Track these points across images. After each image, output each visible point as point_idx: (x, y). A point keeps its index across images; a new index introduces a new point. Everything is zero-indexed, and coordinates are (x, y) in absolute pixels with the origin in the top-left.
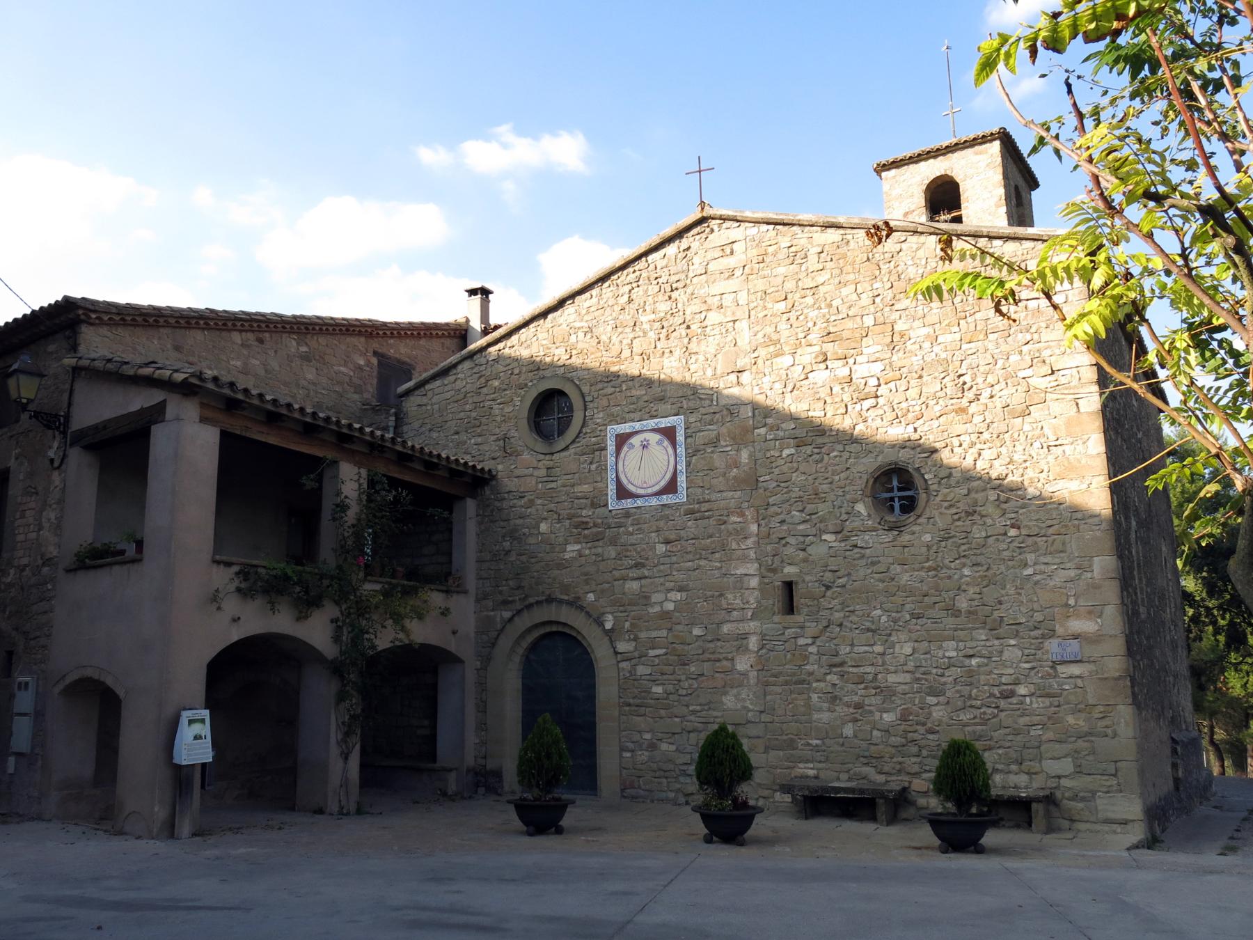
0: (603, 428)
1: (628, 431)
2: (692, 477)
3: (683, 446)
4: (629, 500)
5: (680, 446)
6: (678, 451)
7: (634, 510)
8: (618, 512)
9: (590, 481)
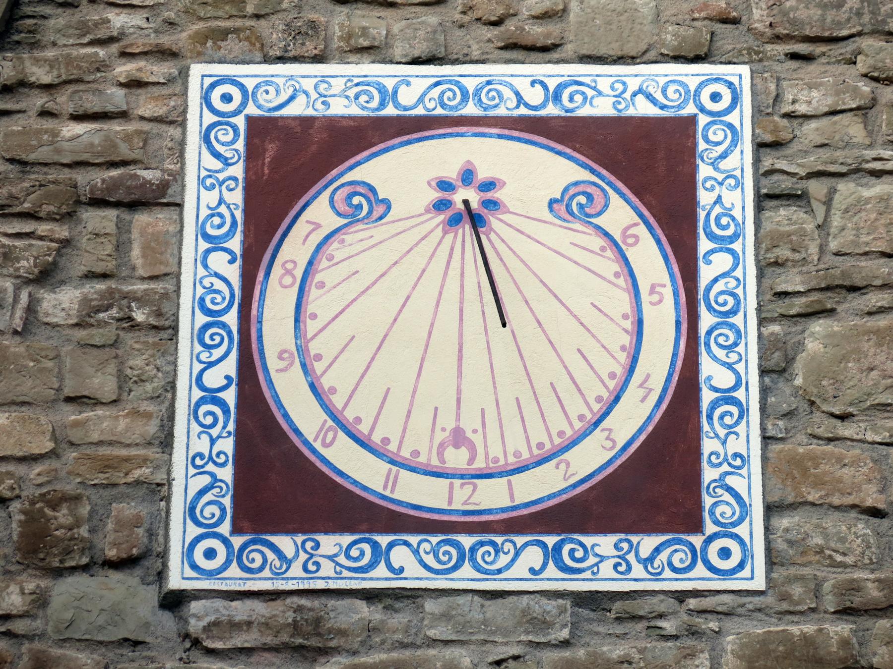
0: (157, 71)
1: (339, 108)
2: (800, 445)
3: (747, 246)
4: (330, 543)
5: (724, 244)
6: (706, 274)
7: (364, 610)
8: (240, 610)
9: (27, 387)
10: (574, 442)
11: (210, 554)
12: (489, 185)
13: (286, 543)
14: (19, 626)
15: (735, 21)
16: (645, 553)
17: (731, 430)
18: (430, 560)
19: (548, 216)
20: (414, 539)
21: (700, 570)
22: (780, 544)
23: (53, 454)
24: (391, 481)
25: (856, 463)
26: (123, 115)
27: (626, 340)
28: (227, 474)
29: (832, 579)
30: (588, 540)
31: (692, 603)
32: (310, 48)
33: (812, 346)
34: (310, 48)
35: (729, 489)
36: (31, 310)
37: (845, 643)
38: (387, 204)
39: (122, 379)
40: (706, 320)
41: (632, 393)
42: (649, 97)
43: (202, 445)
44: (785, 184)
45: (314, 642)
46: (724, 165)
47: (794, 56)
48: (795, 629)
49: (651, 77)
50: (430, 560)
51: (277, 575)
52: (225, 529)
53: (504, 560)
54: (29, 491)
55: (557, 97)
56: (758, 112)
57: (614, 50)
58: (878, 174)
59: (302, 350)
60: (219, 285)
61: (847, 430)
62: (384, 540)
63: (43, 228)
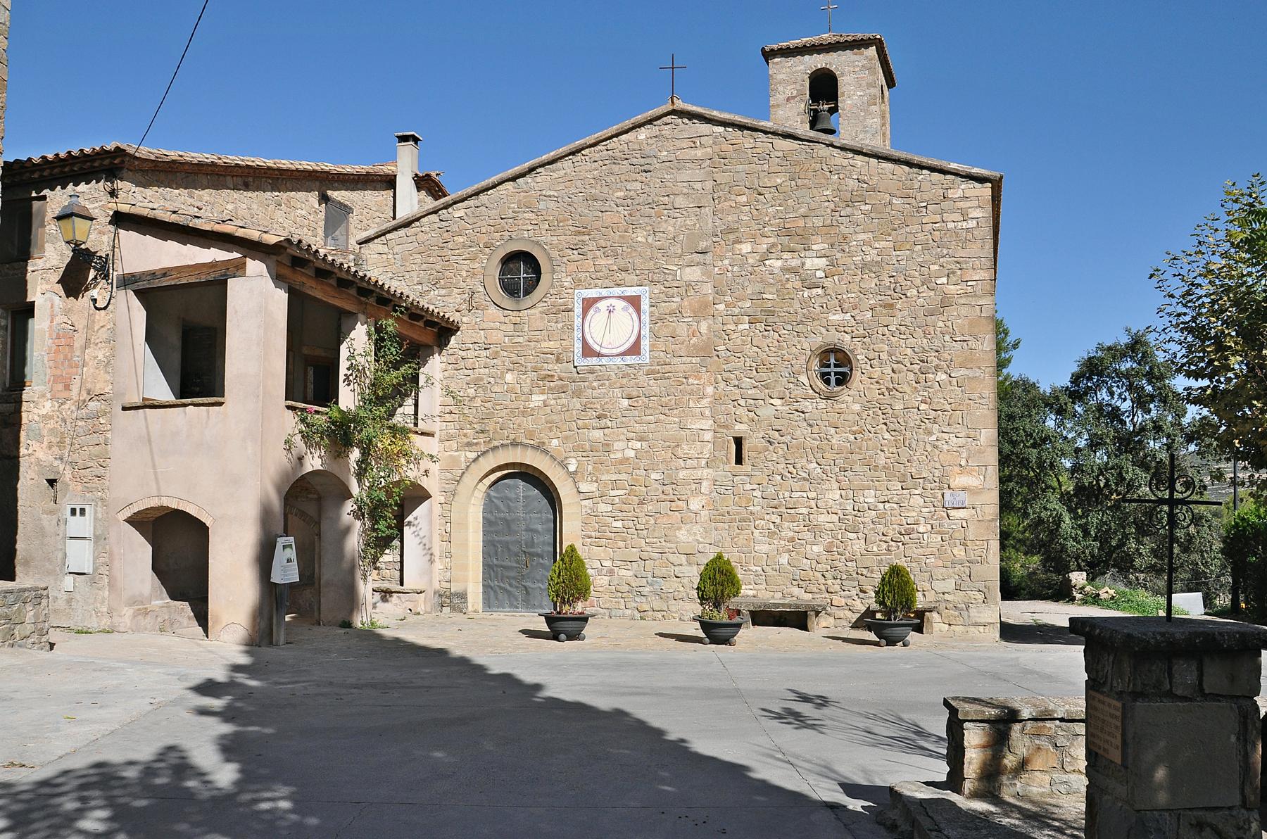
40: (642, 325)
44: (653, 304)
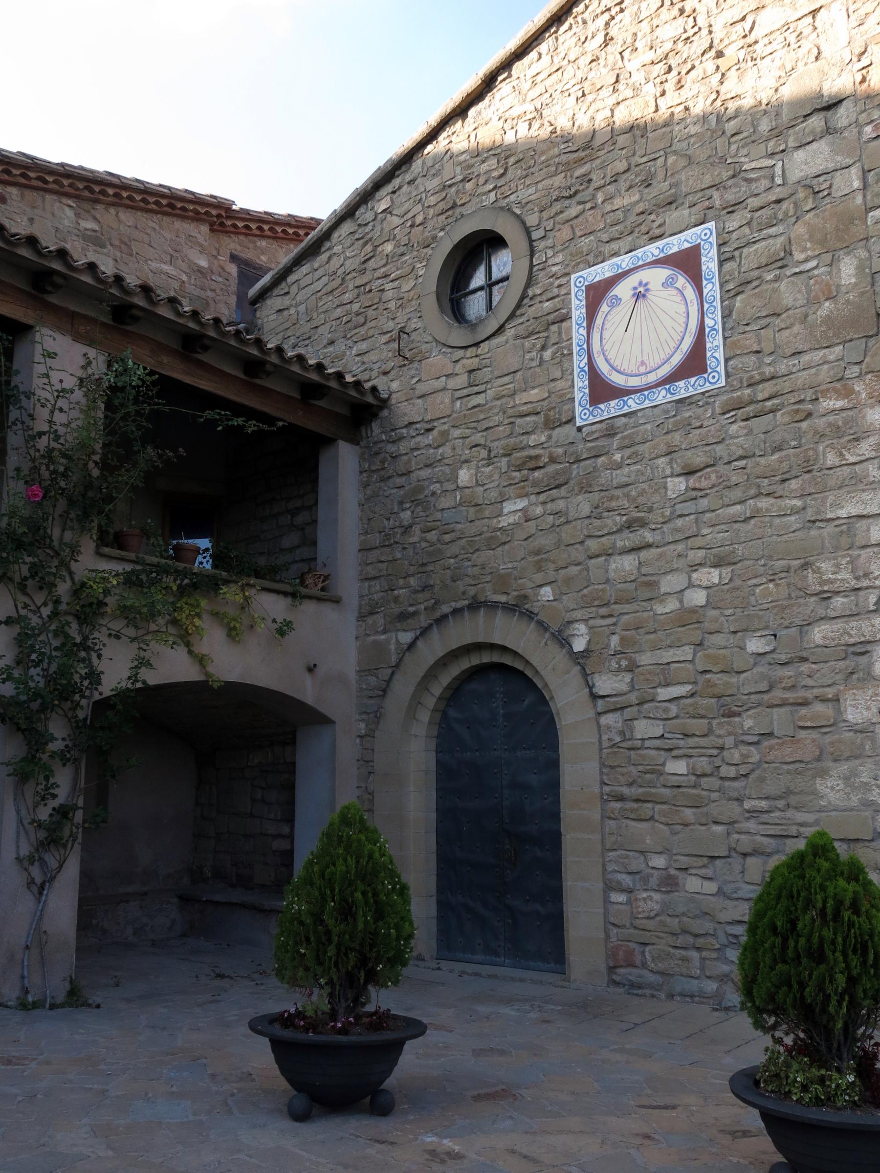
3: (716, 280)
4: (613, 403)
5: (710, 281)
7: (624, 420)
8: (594, 428)
10: (672, 356)
11: (585, 414)
12: (646, 284)
13: (602, 406)
14: (545, 446)
15: (712, 207)
16: (692, 383)
17: (714, 339)
18: (637, 401)
19: (662, 289)
20: (633, 396)
21: (707, 384)
22: (730, 370)
23: (549, 397)
24: (626, 381)
25: (750, 338)
26: (558, 296)
27: (684, 320)
28: (587, 391)
29: (746, 376)
30: (677, 384)
31: (707, 395)
32: (600, 259)
33: (737, 305)
34: (600, 259)
35: (714, 357)
36: (541, 358)
37: (749, 395)
38: (620, 299)
39: (563, 371)
40: (706, 306)
41: (687, 335)
42: (688, 241)
43: (581, 385)
44: (727, 255)
45: (612, 432)
46: (709, 255)
47: (729, 213)
48: (735, 395)
49: (687, 235)
50: (637, 401)
51: (601, 416)
52: (588, 406)
53: (656, 395)
54: (545, 408)
55: (663, 250)
56: (718, 235)
57: (678, 230)
58: (754, 242)
59: (602, 350)
60: (582, 337)
61: (748, 328)
62: (625, 399)
63: (541, 335)
